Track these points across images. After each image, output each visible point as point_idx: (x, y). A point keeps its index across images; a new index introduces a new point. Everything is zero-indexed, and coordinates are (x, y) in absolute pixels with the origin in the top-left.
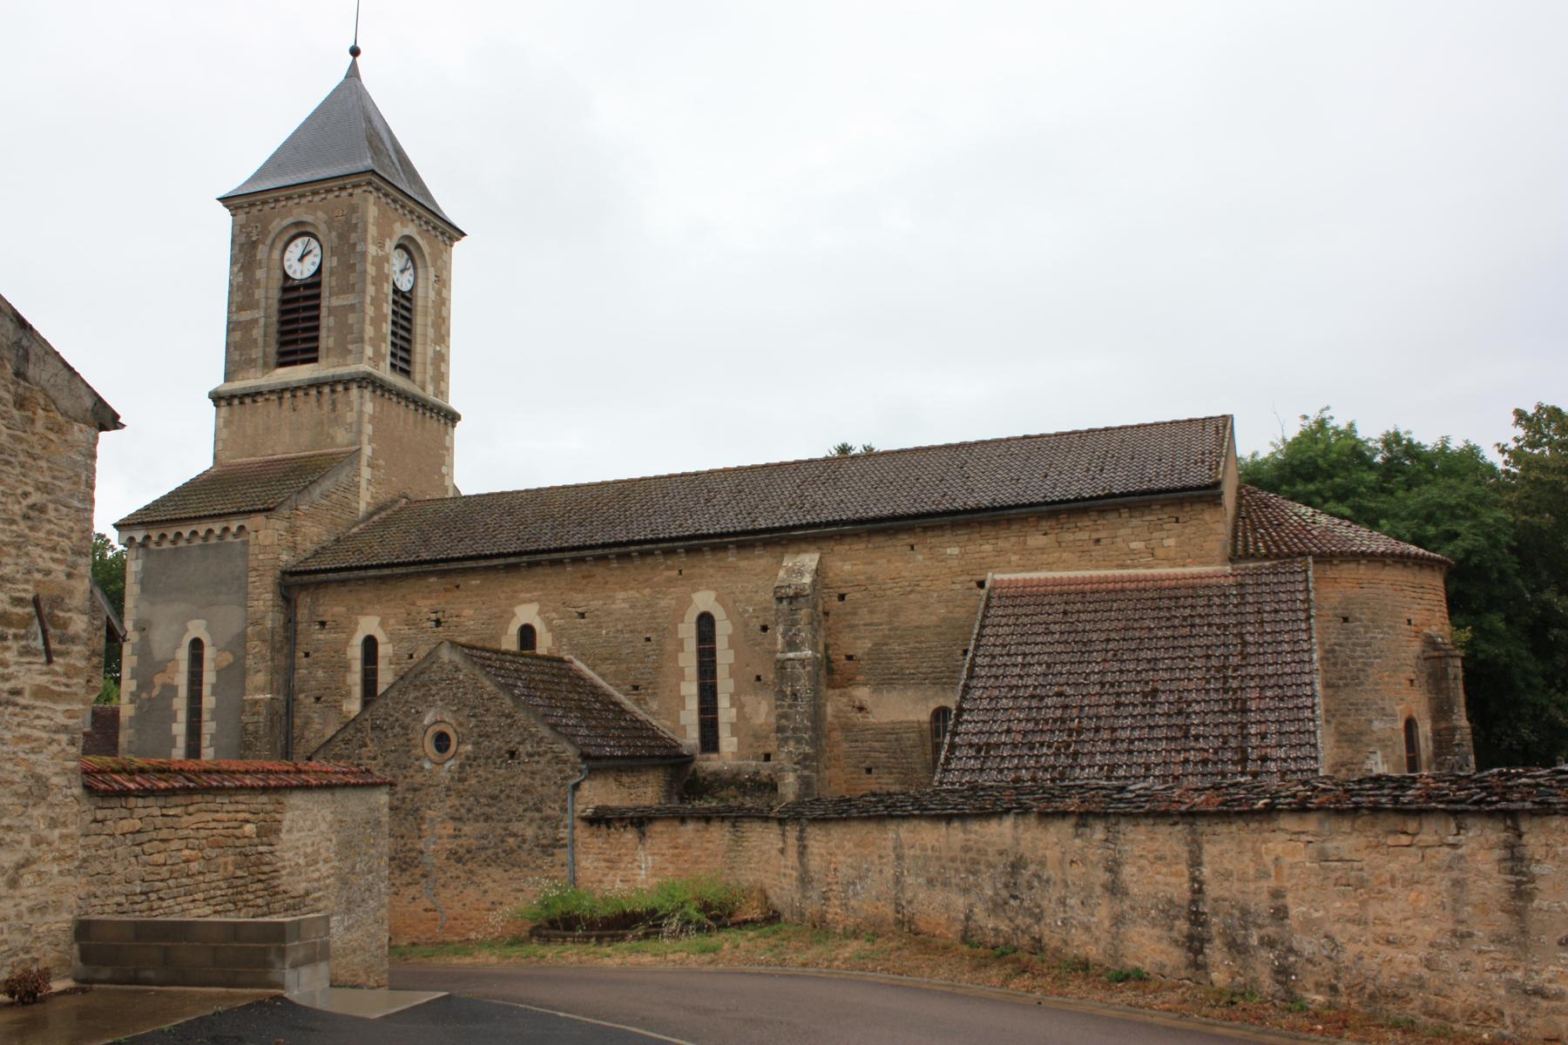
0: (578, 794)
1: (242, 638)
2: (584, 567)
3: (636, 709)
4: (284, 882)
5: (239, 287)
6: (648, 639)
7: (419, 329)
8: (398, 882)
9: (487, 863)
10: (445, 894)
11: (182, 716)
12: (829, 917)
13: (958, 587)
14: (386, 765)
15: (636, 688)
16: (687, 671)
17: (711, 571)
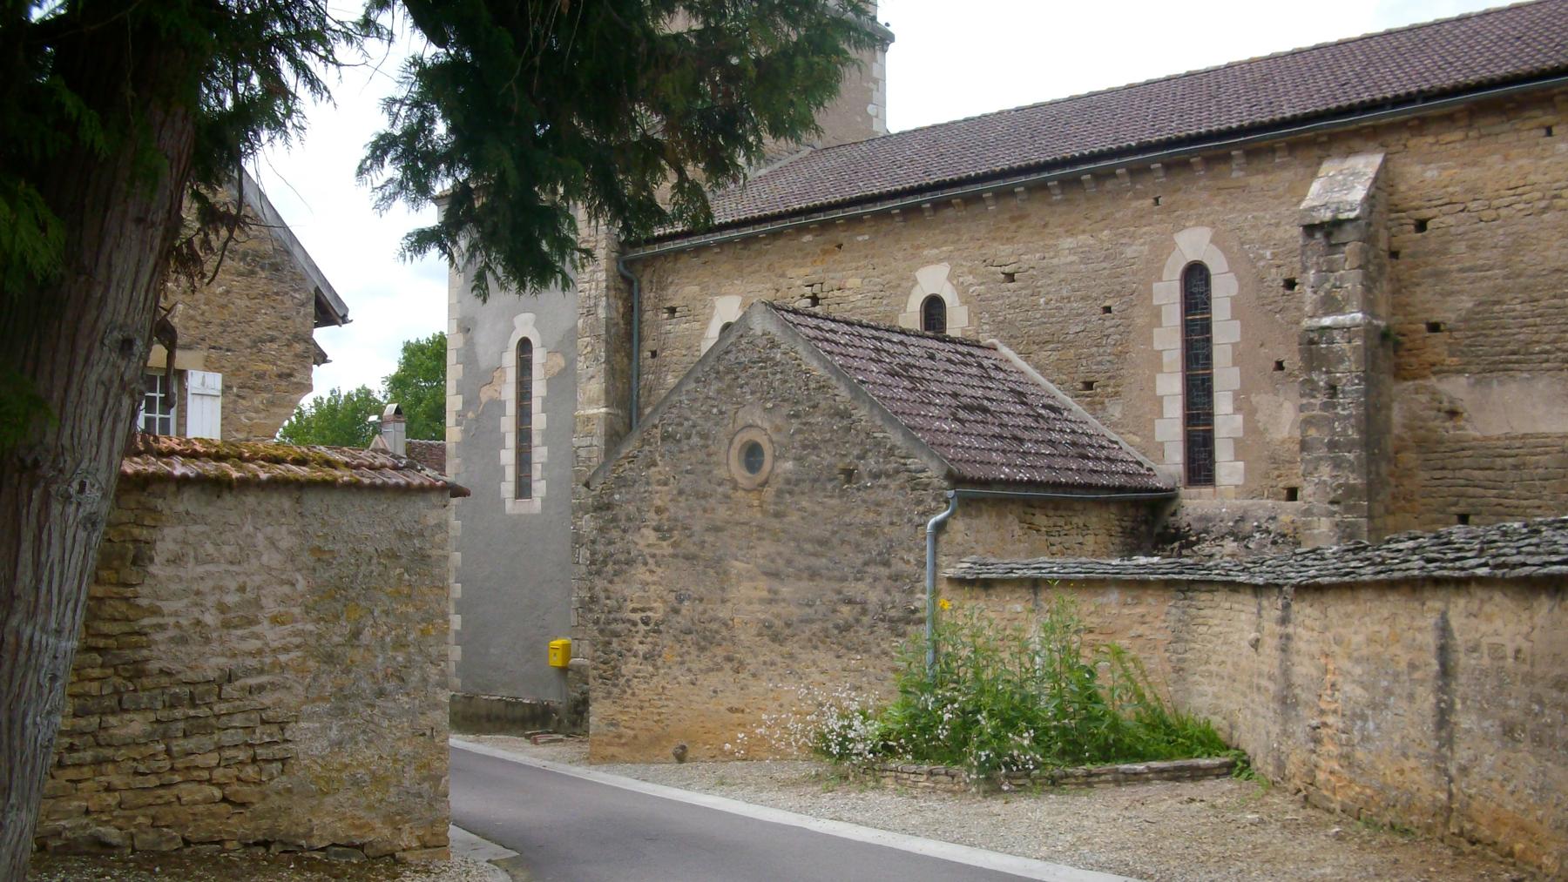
0: (944, 538)
1: (572, 335)
2: (1014, 202)
3: (1088, 416)
4: (160, 654)
6: (1108, 310)
8: (695, 667)
11: (511, 440)
12: (1321, 776)
14: (681, 492)
15: (1089, 385)
16: (1166, 358)
17: (1205, 196)
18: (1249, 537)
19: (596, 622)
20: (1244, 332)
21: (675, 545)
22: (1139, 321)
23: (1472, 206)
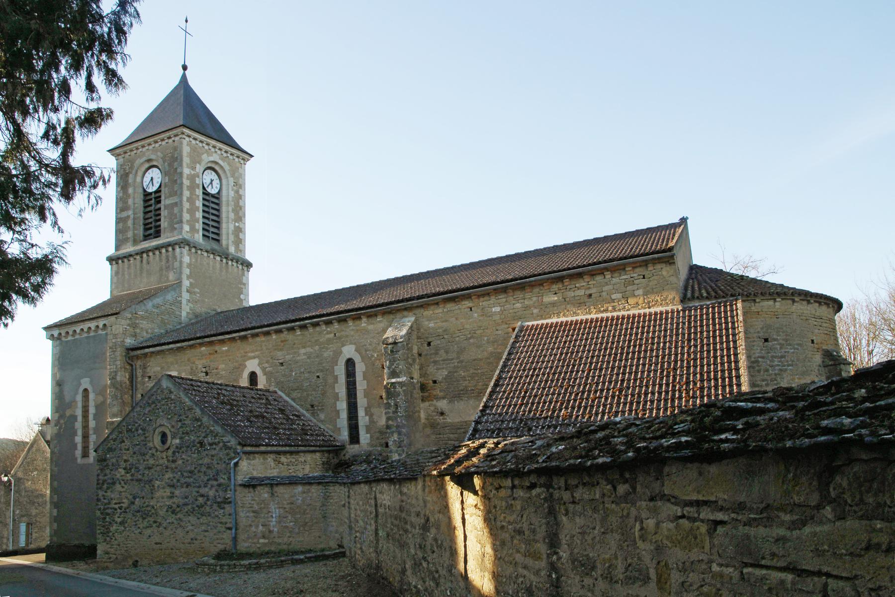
3: (312, 419)
5: (121, 199)
6: (318, 377)
7: (224, 215)
8: (141, 526)
9: (188, 514)
10: (167, 533)
13: (500, 332)
14: (134, 453)
15: (312, 406)
18: (371, 462)
19: (99, 509)
20: (368, 386)
21: (132, 475)
22: (329, 381)
23: (446, 336)
